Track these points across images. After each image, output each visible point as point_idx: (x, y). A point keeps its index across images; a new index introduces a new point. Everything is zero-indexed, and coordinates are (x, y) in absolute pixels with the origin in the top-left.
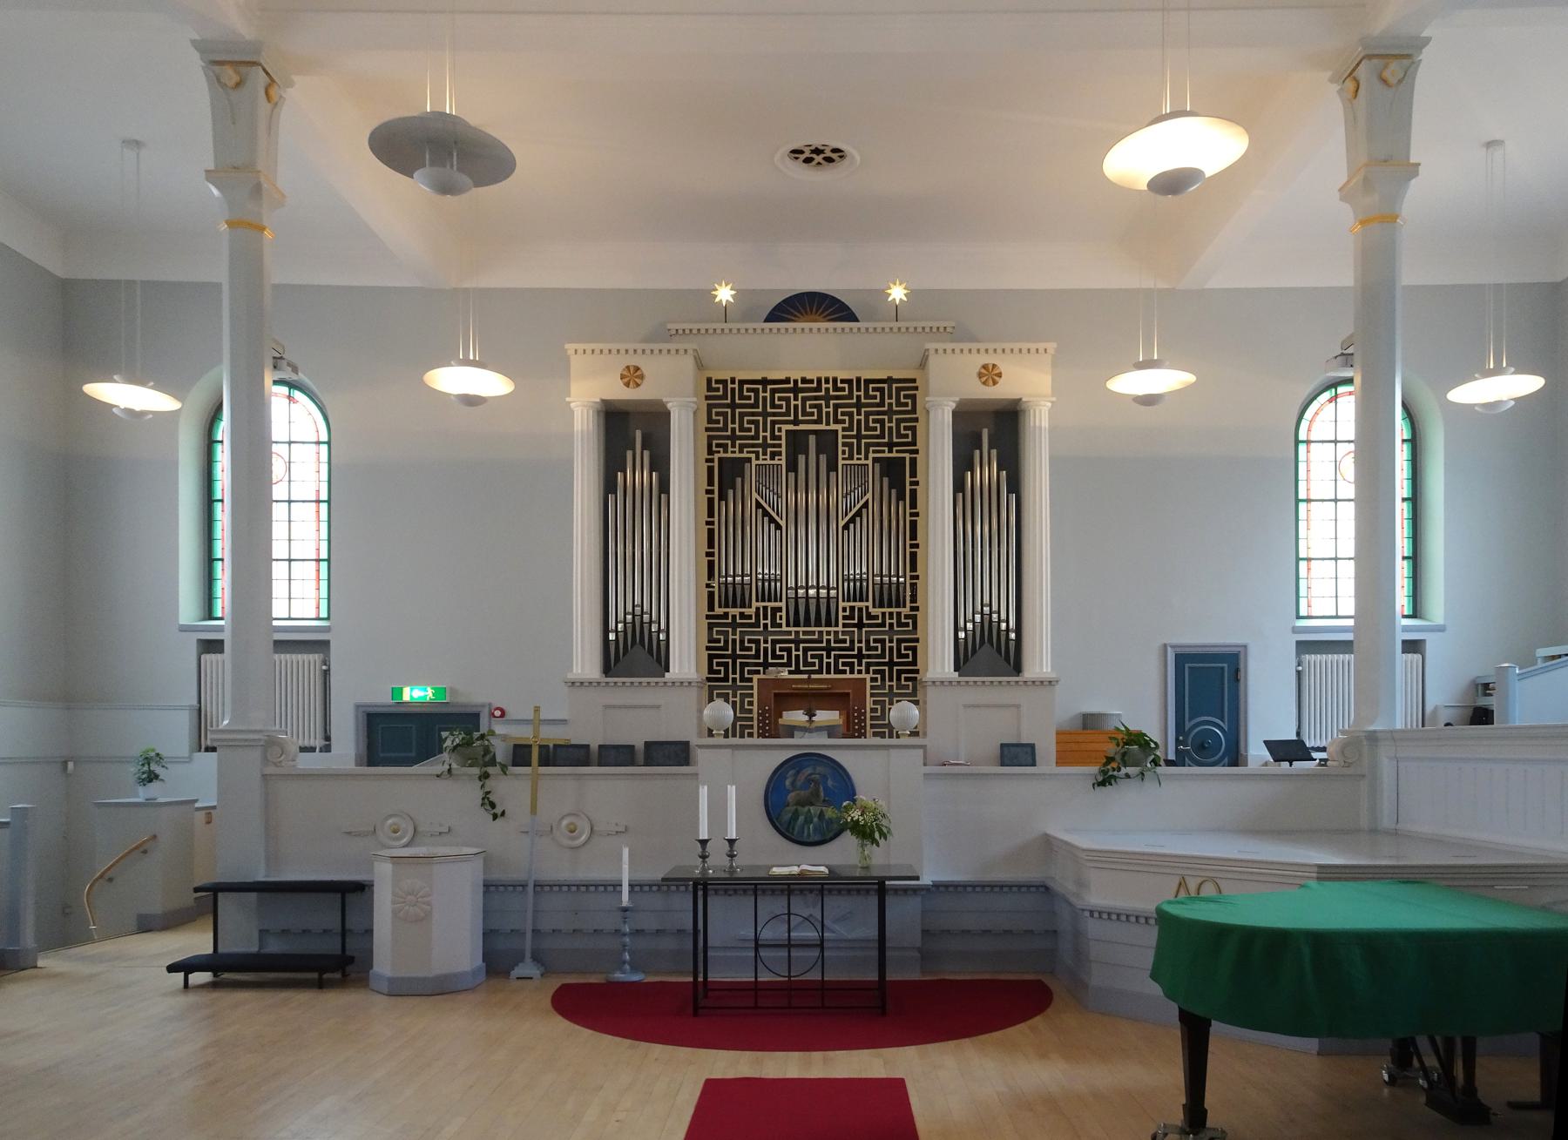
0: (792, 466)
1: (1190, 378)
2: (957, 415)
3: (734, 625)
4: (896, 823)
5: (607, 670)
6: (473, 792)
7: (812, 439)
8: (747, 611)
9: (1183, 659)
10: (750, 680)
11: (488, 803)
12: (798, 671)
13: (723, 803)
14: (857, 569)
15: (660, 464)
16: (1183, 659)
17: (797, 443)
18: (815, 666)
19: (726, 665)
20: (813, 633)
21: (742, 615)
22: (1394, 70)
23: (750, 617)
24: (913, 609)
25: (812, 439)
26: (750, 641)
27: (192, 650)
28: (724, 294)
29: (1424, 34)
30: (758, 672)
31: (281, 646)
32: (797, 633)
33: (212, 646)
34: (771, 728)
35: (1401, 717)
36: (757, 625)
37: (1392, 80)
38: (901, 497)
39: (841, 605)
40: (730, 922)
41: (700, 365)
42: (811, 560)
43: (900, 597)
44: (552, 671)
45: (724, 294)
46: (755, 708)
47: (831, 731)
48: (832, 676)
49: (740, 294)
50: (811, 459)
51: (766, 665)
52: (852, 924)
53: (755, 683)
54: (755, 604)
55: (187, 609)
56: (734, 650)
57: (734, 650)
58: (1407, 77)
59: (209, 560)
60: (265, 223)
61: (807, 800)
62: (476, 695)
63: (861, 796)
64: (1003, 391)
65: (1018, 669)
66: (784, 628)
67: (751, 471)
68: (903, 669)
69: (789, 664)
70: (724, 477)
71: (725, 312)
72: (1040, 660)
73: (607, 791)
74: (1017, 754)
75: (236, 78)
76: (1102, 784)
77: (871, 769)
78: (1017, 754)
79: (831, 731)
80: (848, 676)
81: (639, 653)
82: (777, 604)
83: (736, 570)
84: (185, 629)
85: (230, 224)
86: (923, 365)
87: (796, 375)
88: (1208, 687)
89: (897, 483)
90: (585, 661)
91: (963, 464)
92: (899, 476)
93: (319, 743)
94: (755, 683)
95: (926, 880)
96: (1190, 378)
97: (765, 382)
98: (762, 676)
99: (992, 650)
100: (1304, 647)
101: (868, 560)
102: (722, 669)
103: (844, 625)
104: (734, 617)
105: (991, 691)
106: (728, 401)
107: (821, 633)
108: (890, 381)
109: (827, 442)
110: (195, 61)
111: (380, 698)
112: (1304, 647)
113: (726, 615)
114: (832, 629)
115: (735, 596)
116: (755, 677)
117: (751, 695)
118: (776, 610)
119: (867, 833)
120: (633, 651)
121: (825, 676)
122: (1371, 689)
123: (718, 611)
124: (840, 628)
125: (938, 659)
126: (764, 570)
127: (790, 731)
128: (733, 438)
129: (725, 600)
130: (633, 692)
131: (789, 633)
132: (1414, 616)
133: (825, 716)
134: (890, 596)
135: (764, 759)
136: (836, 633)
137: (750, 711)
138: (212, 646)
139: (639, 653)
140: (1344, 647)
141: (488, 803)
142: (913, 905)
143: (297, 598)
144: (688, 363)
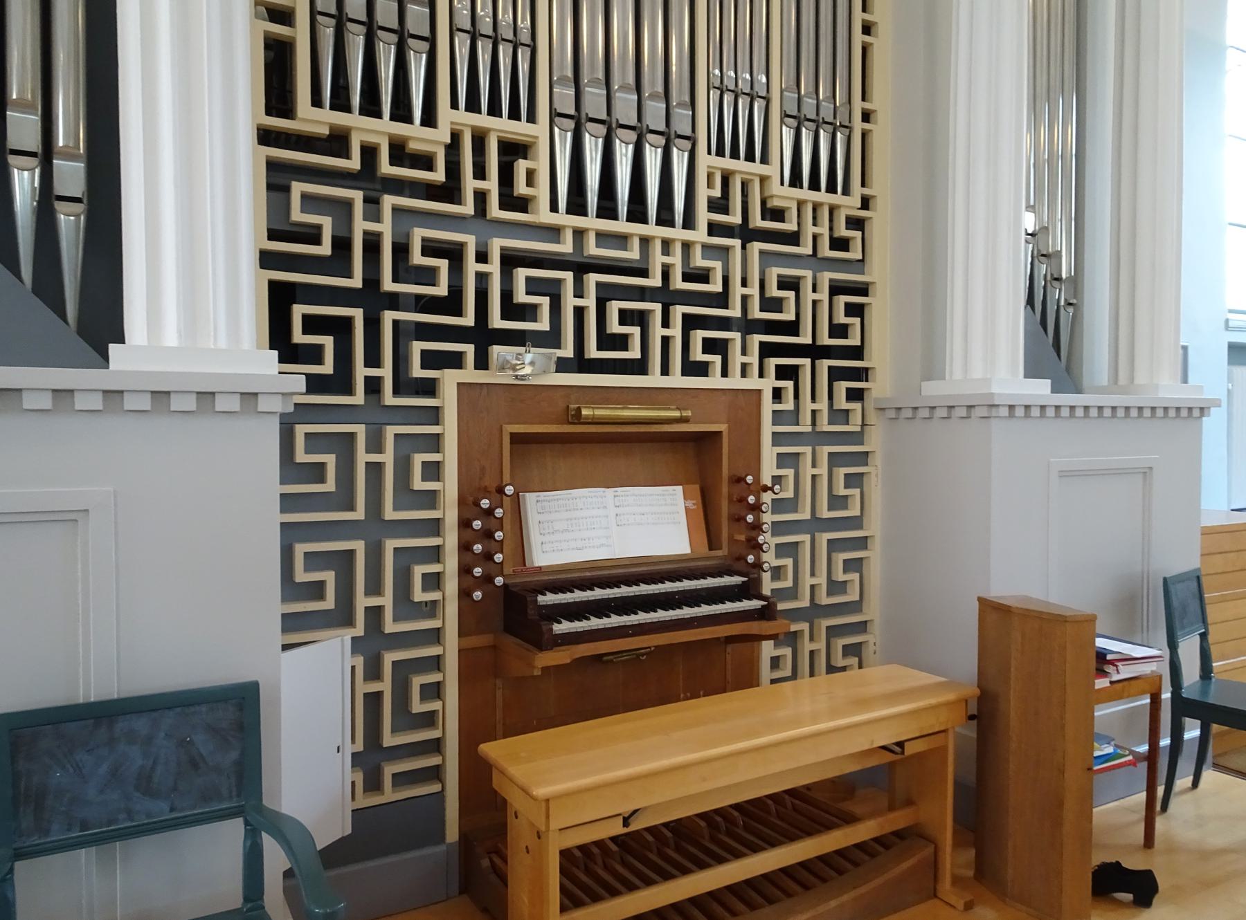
1: (263, 834)
3: (581, 268)
7: (436, 788)
8: (416, 135)
10: (429, 388)
12: (581, 364)
19: (341, 328)
20: (621, 240)
21: (399, 153)
23: (426, 162)
24: (866, 203)
25: (436, 788)
26: (431, 248)
30: (455, 361)
32: (579, 234)
36: (449, 191)
39: (705, 161)
46: (450, 487)
48: (677, 380)
51: (483, 337)
53: (448, 399)
54: (446, 115)
56: (373, 326)
57: (373, 326)
66: (543, 215)
69: (551, 339)
80: (714, 381)
82: (519, 129)
94: (448, 399)
96: (263, 834)
98: (469, 374)
103: (713, 229)
104: (369, 153)
107: (645, 241)
113: (337, 142)
114: (677, 233)
116: (449, 379)
117: (435, 443)
118: (513, 150)
121: (654, 379)
123: (312, 118)
124: (700, 235)
131: (554, 232)
136: (687, 246)
137: (431, 499)
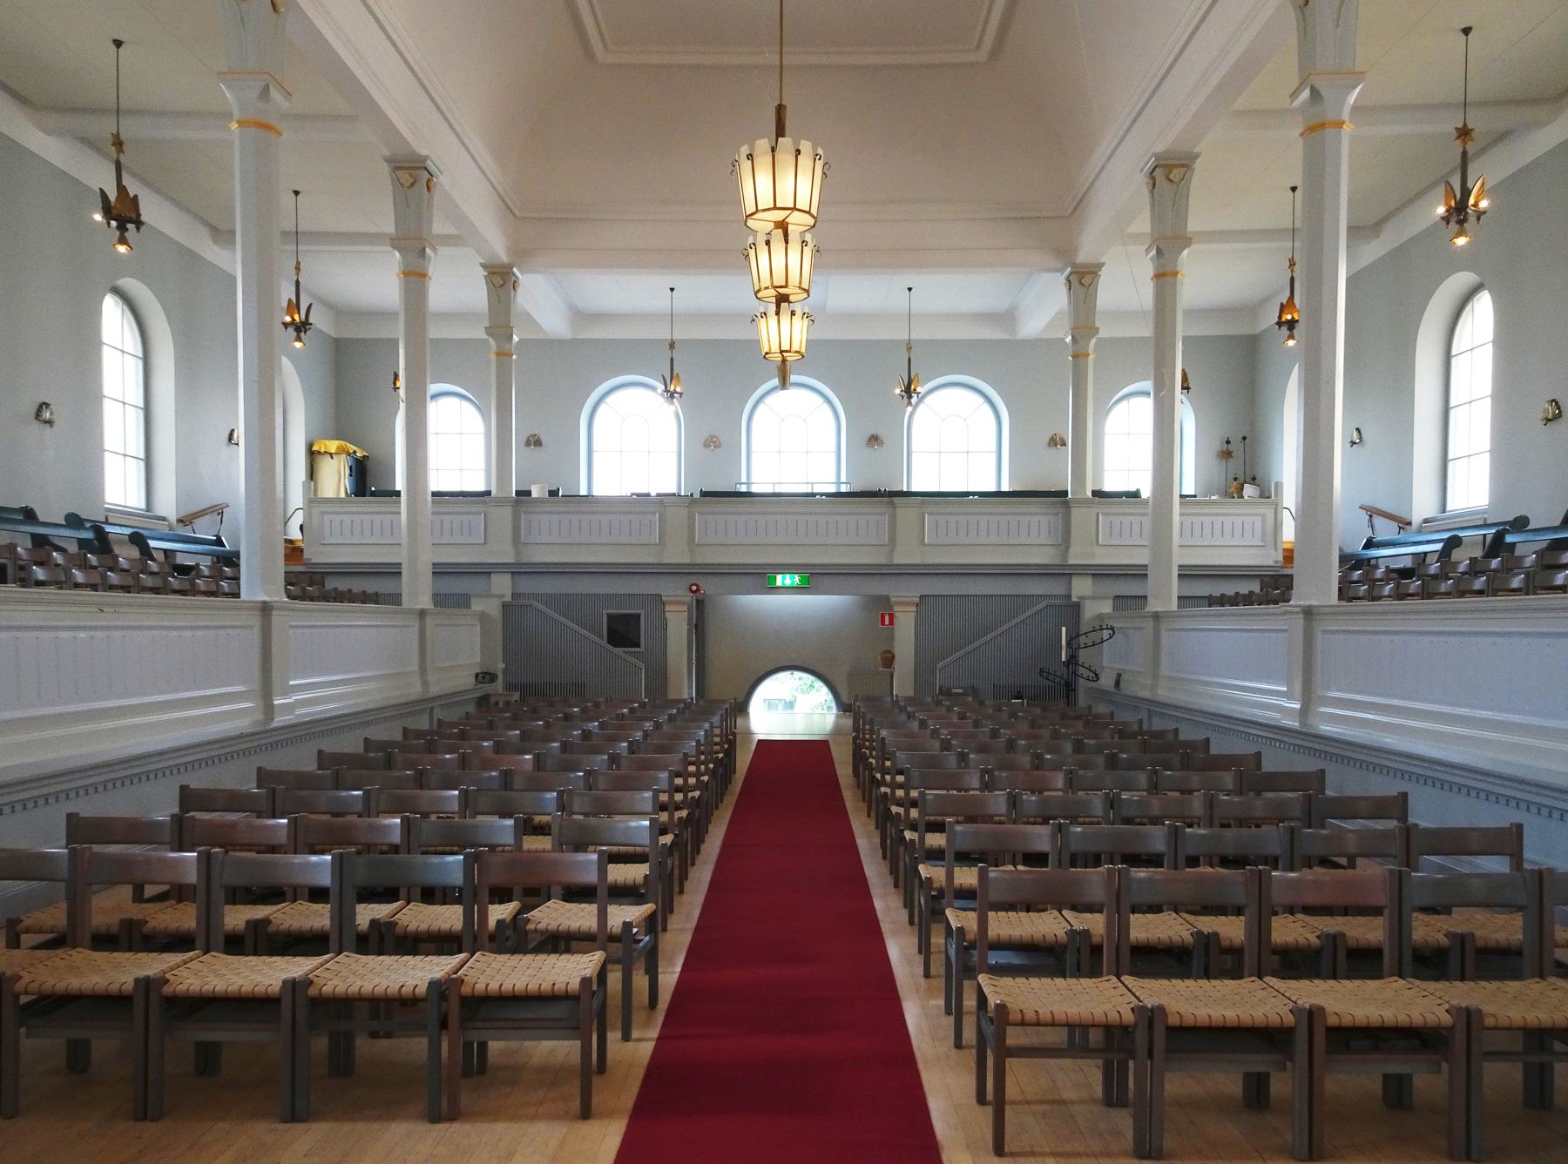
29: (1196, 150)
110: (386, 168)
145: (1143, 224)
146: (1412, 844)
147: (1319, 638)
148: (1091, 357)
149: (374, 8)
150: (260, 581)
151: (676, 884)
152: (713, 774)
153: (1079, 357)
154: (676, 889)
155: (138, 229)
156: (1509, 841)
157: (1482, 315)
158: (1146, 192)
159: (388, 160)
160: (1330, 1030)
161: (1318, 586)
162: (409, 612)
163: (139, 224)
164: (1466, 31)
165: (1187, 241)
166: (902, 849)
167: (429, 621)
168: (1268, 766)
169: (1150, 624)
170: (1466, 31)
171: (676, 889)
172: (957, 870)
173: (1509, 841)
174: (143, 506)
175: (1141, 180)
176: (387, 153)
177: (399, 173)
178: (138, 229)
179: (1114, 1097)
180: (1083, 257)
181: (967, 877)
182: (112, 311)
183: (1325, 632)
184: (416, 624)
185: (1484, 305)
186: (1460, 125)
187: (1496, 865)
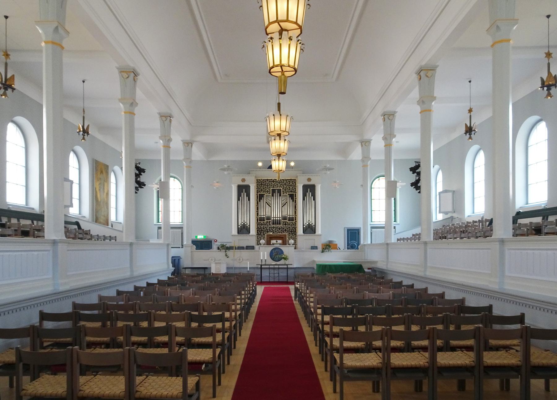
0: (273, 195)
2: (303, 186)
3: (262, 225)
4: (290, 257)
5: (238, 233)
6: (224, 254)
9: (348, 230)
11: (226, 255)
13: (264, 254)
14: (285, 214)
15: (248, 195)
16: (348, 230)
17: (274, 191)
18: (278, 232)
22: (391, 117)
27: (157, 229)
28: (260, 164)
29: (437, 64)
31: (172, 228)
33: (160, 228)
34: (268, 243)
35: (394, 240)
37: (429, 76)
38: (293, 201)
40: (265, 273)
41: (256, 177)
42: (276, 210)
43: (293, 219)
44: (230, 234)
45: (260, 164)
47: (280, 244)
49: (263, 164)
50: (276, 194)
52: (283, 273)
55: (155, 222)
58: (433, 76)
59: (158, 211)
60: (135, 113)
61: (276, 255)
62: (212, 237)
63: (285, 253)
64: (311, 183)
65: (315, 233)
67: (265, 196)
68: (293, 232)
70: (260, 197)
71: (260, 168)
72: (319, 231)
73: (245, 254)
74: (314, 248)
75: (127, 76)
76: (323, 252)
77: (287, 250)
78: (314, 248)
79: (280, 244)
81: (244, 230)
83: (262, 214)
84: (155, 225)
85: (125, 113)
86: (297, 177)
87: (273, 179)
88: (353, 236)
89: (292, 198)
90: (235, 231)
91: (304, 195)
92: (293, 197)
93: (181, 246)
95: (295, 266)
97: (267, 180)
99: (310, 229)
100: (372, 228)
101: (288, 212)
102: (260, 232)
105: (310, 237)
106: (261, 184)
108: (291, 180)
109: (279, 191)
110: (117, 71)
111: (194, 238)
112: (372, 228)
115: (262, 219)
119: (285, 259)
120: (243, 230)
122: (388, 235)
125: (300, 231)
126: (268, 214)
127: (273, 244)
128: (262, 190)
129: (260, 220)
130: (244, 237)
132: (395, 221)
133: (280, 241)
134: (291, 219)
135: (270, 248)
138: (160, 228)
139: (244, 230)
140: (383, 228)
141: (226, 255)
142: (293, 270)
143: (176, 218)
144: (254, 177)
145: (415, 94)
146: (530, 334)
147: (389, 249)
148: (369, 167)
149: (109, 3)
150: (53, 230)
151: (238, 329)
152: (249, 298)
153: (365, 166)
154: (226, 362)
155: (13, 91)
156: (521, 319)
157: (481, 156)
158: (417, 80)
159: (118, 68)
160: (438, 368)
161: (503, 229)
162: (48, 242)
163: (88, 134)
164: (548, 16)
165: (434, 98)
166: (318, 332)
167: (429, 246)
168: (496, 312)
169: (497, 245)
170: (548, 16)
171: (226, 362)
172: (325, 316)
173: (521, 319)
174: (25, 204)
175: (415, 77)
176: (117, 66)
177: (122, 73)
178: (13, 91)
179: (376, 389)
180: (366, 137)
181: (336, 329)
182: (72, 156)
183: (509, 249)
184: (128, 248)
185: (482, 153)
186: (547, 51)
187: (518, 326)
